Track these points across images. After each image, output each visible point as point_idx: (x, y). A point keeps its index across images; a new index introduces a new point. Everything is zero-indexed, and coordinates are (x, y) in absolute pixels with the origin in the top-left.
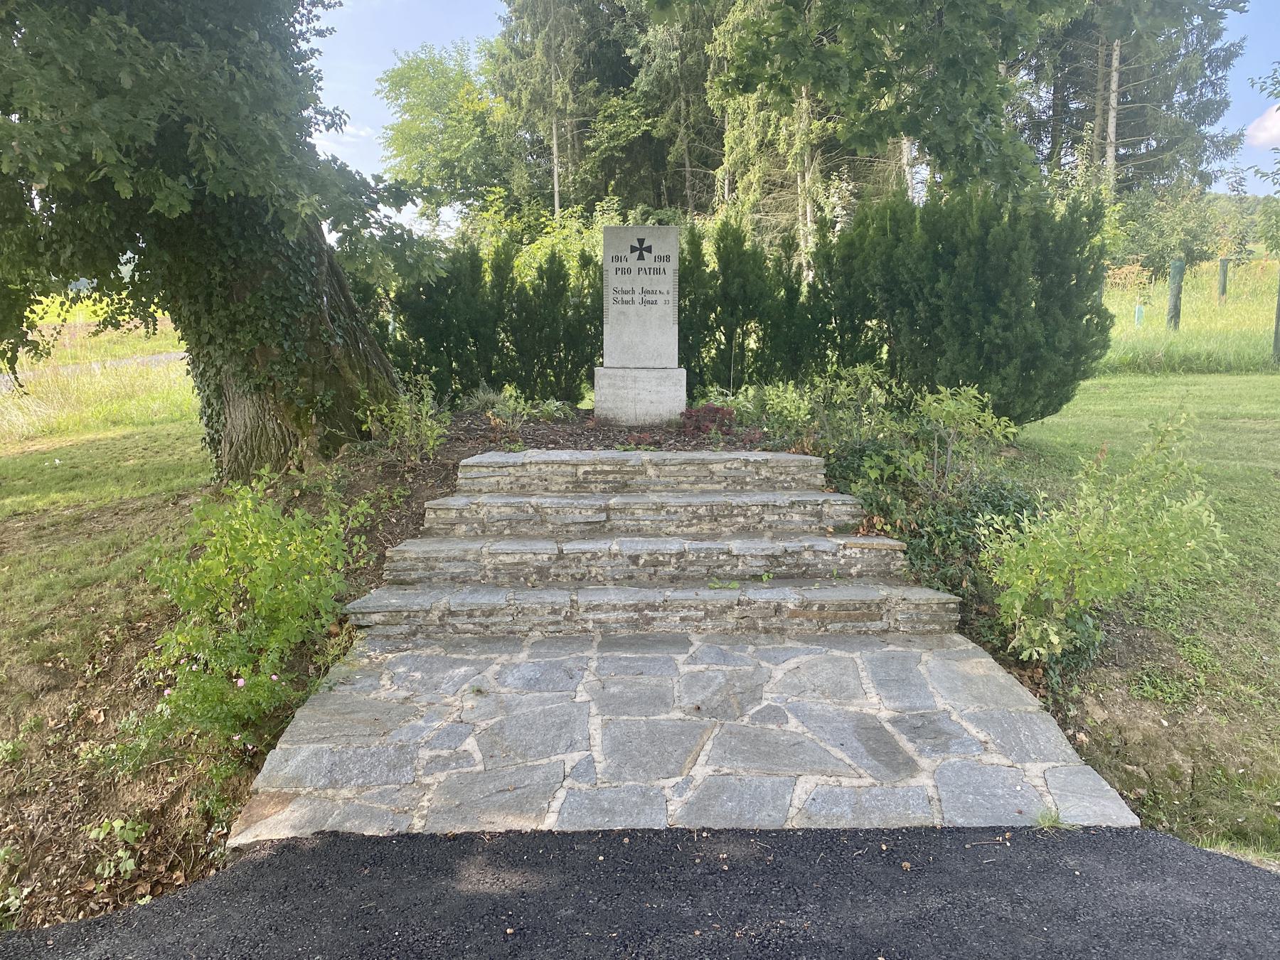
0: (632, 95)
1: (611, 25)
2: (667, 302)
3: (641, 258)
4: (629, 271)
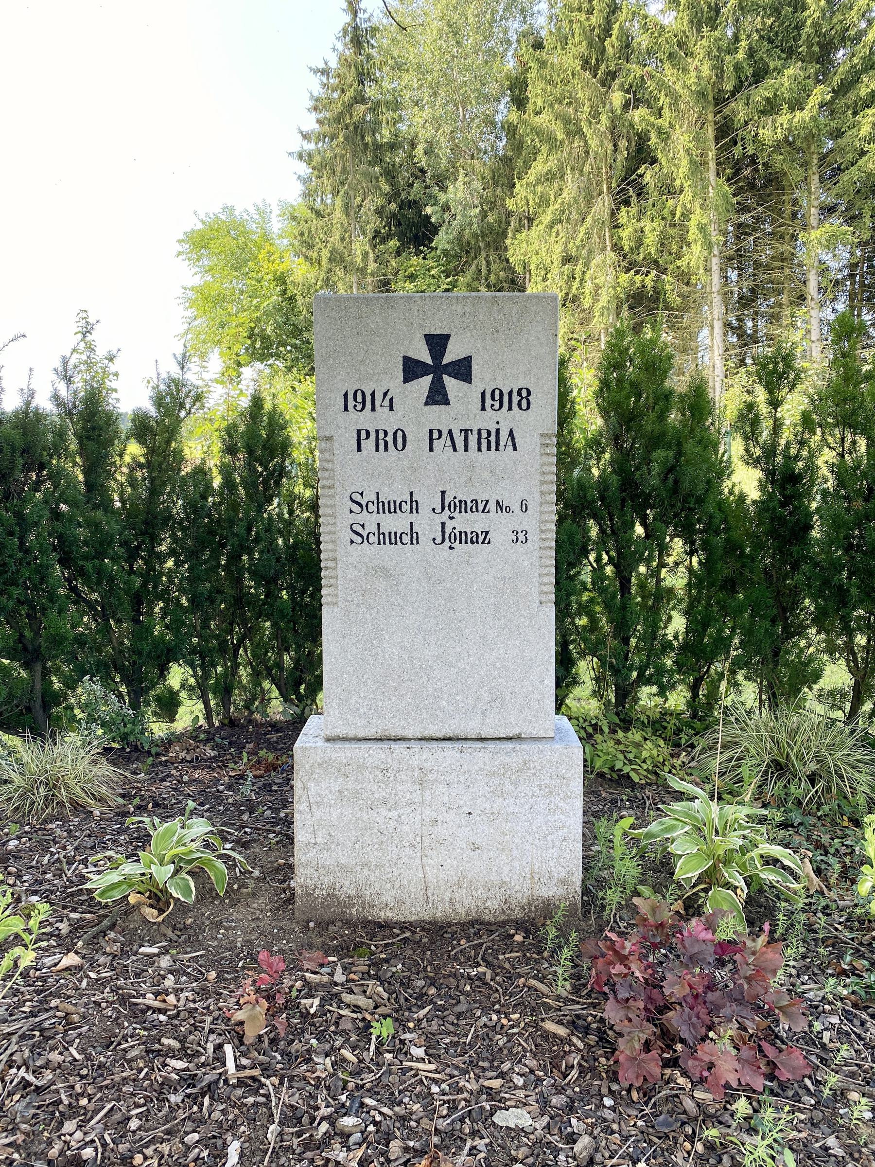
0: (433, 253)
1: (411, 185)
2: (519, 537)
3: (438, 396)
4: (400, 439)
